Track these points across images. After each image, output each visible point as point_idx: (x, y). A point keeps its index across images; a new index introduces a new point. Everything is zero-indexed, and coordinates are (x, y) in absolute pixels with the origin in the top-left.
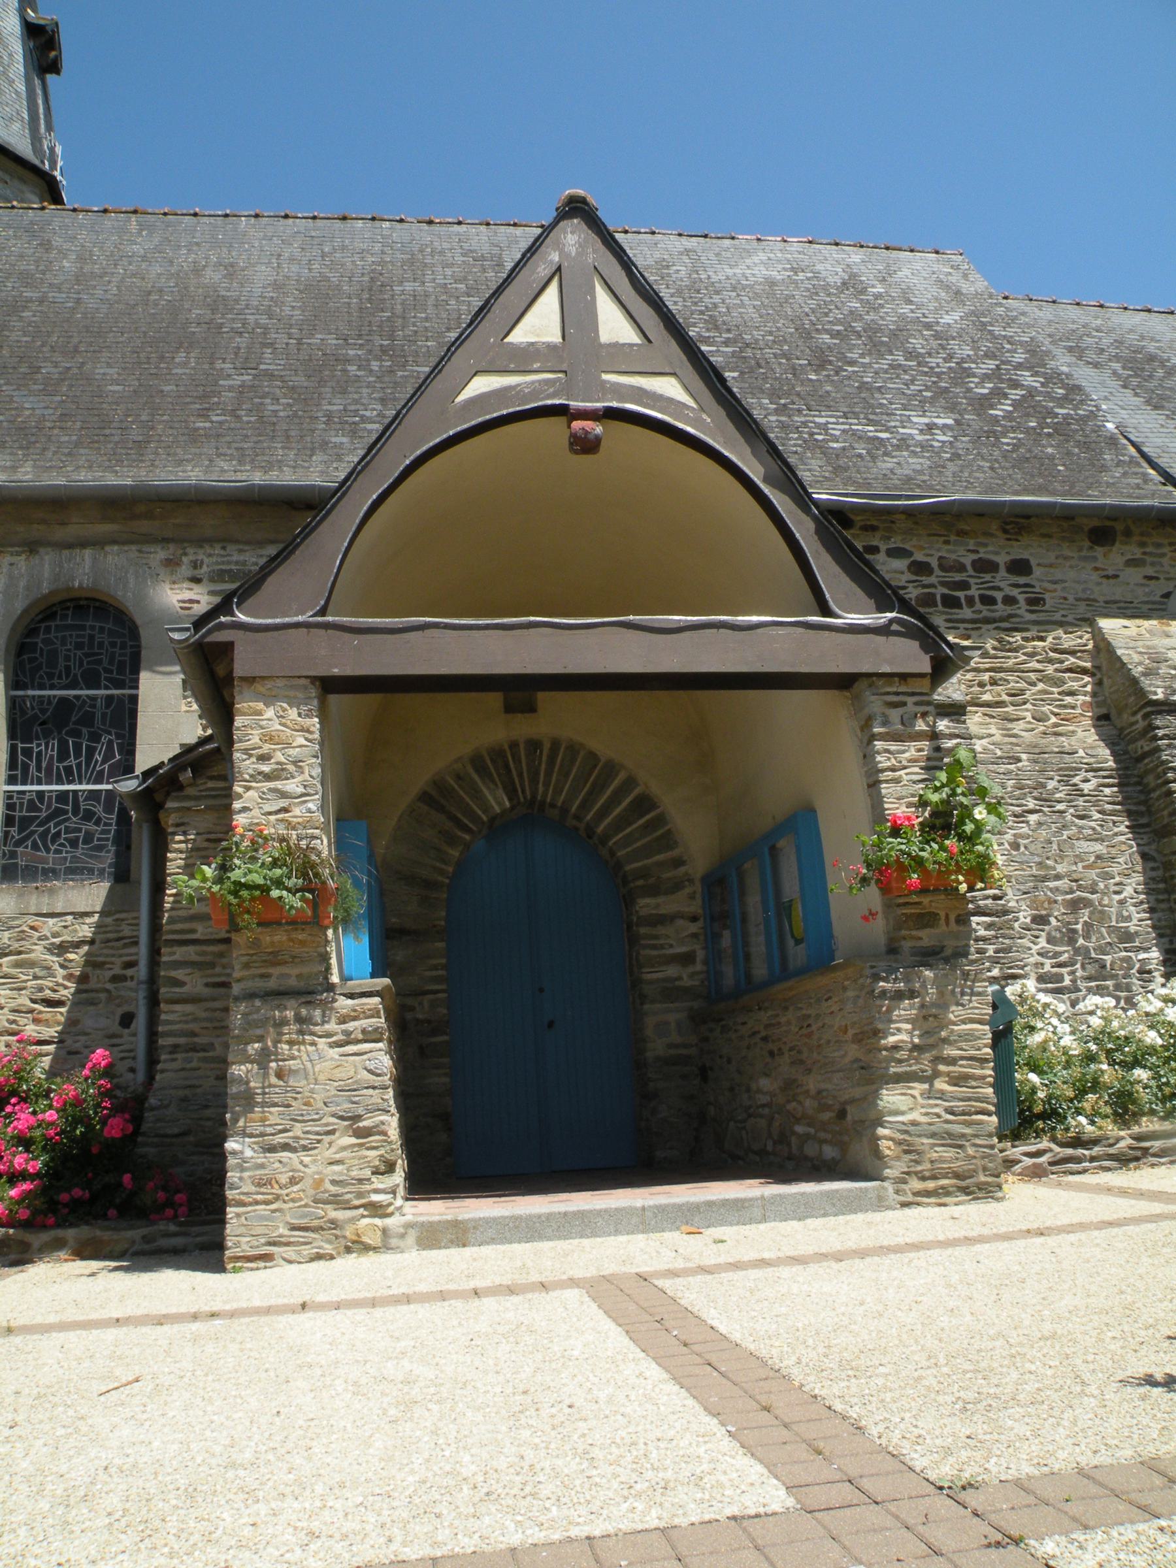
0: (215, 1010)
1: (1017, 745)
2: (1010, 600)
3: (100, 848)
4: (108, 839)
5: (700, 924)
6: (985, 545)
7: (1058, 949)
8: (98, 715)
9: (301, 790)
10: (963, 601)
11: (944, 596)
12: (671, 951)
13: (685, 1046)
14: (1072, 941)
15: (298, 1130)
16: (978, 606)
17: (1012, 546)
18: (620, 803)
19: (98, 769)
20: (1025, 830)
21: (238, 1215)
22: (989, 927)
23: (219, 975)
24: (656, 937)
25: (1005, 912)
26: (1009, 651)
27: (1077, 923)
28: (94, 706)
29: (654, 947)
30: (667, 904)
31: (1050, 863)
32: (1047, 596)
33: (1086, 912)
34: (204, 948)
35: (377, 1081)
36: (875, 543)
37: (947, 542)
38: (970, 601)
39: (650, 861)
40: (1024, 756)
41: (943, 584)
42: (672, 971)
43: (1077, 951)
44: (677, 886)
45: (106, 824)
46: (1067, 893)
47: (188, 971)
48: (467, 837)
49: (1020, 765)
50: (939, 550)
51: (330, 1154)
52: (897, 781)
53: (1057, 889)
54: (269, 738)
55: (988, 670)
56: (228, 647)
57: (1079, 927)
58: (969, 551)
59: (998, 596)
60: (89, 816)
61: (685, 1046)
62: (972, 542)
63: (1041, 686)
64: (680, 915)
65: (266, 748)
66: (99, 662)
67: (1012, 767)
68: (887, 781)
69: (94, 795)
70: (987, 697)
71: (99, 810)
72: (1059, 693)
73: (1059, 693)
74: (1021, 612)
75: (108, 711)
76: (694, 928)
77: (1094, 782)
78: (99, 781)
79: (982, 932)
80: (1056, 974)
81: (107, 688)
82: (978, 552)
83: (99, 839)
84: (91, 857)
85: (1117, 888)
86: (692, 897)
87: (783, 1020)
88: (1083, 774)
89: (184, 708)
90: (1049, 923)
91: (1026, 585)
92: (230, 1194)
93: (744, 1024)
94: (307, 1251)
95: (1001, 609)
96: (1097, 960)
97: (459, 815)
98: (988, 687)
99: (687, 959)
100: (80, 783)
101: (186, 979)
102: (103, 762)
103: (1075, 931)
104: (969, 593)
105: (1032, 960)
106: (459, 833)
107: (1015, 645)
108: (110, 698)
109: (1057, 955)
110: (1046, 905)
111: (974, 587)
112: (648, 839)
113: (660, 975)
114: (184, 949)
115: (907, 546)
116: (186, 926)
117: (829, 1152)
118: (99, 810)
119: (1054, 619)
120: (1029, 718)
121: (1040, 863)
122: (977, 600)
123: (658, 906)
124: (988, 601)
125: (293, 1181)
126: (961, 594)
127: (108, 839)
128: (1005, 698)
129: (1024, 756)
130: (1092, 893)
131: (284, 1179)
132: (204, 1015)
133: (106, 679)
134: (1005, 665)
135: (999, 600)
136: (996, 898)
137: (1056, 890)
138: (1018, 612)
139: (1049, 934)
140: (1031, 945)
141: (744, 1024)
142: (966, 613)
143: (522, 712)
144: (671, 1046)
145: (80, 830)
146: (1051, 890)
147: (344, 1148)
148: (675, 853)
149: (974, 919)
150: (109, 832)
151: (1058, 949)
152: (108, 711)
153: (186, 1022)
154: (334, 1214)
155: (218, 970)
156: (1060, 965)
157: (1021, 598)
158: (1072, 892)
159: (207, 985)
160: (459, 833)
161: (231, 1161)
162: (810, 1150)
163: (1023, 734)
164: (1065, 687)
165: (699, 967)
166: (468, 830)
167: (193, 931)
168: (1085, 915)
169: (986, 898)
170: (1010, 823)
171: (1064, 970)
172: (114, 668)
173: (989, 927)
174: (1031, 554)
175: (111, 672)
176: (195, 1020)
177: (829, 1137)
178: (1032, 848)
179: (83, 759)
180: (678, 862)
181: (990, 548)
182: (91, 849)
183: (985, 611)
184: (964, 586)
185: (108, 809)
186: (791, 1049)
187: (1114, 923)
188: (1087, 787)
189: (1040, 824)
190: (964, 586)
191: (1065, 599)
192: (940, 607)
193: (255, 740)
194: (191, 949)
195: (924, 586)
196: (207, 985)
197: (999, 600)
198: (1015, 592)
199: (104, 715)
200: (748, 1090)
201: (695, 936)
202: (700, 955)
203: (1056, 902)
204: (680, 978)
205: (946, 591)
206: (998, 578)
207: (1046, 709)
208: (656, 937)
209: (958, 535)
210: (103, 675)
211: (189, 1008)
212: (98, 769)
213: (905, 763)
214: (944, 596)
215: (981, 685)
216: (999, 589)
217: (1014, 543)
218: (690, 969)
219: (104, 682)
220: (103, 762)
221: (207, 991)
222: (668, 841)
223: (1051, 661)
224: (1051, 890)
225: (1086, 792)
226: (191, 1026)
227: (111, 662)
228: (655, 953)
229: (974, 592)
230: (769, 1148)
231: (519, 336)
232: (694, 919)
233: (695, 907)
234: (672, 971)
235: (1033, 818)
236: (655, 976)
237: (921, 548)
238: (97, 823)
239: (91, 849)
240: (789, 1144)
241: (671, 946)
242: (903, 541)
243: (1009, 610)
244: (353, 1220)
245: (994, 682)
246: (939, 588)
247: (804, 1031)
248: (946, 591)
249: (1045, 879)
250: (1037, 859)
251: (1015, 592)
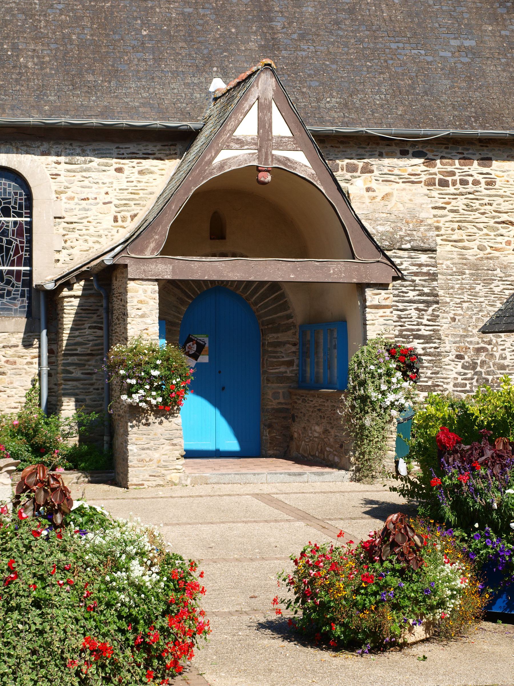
0: (86, 385)
1: (465, 265)
2: (476, 183)
3: (14, 299)
4: (18, 294)
5: (297, 347)
6: (468, 150)
7: (466, 371)
8: (10, 232)
9: (152, 322)
10: (450, 183)
11: (440, 180)
12: (283, 360)
13: (286, 404)
14: (474, 368)
15: (152, 443)
16: (458, 186)
17: (483, 150)
18: (263, 287)
19: (12, 259)
20: (460, 312)
21: (132, 471)
22: (429, 361)
23: (88, 370)
24: (276, 352)
25: (439, 354)
26: (471, 211)
27: (478, 359)
28: (7, 226)
29: (275, 357)
30: (282, 337)
31: (470, 329)
32: (498, 180)
33: (484, 354)
34: (81, 358)
35: (178, 428)
36: (407, 149)
37: (447, 148)
38: (454, 183)
39: (276, 316)
40: (467, 272)
41: (440, 172)
42: (282, 369)
43: (476, 373)
44: (288, 328)
45: (17, 287)
46: (476, 344)
47: (74, 367)
48: (190, 301)
49: (464, 276)
50: (441, 152)
51: (163, 452)
52: (373, 324)
53: (471, 342)
54: (141, 302)
55: (457, 222)
56: (126, 266)
57: (479, 362)
58: (458, 153)
59: (470, 179)
60: (8, 282)
61: (286, 404)
62: (460, 148)
63: (485, 231)
64: (288, 342)
65: (140, 306)
66: (10, 203)
67: (459, 277)
68: (370, 325)
69: (10, 272)
70: (454, 237)
71: (13, 280)
72: (495, 236)
73: (495, 236)
74: (482, 189)
75: (15, 229)
76: (294, 349)
77: (502, 287)
78: (12, 265)
79: (426, 364)
80: (463, 383)
81: (14, 217)
82: (463, 154)
83: (14, 294)
84: (10, 303)
85: (502, 343)
86: (295, 334)
87: (326, 404)
88: (496, 283)
89: (55, 232)
90: (464, 359)
91: (487, 174)
92: (130, 464)
93: (312, 401)
94: (155, 483)
95: (470, 187)
96: (485, 378)
97: (187, 291)
98: (457, 231)
99: (290, 363)
100: (4, 266)
101: (73, 371)
102: (14, 256)
103: (477, 363)
104: (454, 178)
105: (452, 376)
106: (187, 300)
107: (474, 208)
108: (15, 223)
109: (465, 374)
110: (464, 350)
111: (458, 174)
112: (274, 306)
113: (277, 371)
114: (72, 357)
115: (424, 150)
116: (73, 347)
117: (337, 459)
118: (13, 280)
119: (498, 193)
120: (476, 249)
121: (465, 329)
122: (458, 182)
123: (278, 338)
124: (464, 182)
125: (151, 460)
126: (449, 179)
127: (18, 294)
128: (465, 237)
129: (467, 272)
130: (489, 345)
131: (148, 460)
132: (82, 386)
133: (13, 212)
134: (467, 219)
135: (470, 182)
136: (435, 348)
137: (471, 343)
138: (479, 189)
139: (463, 364)
140: (453, 369)
141: (312, 401)
142: (451, 189)
143: (219, 239)
144: (279, 403)
145: (5, 290)
146: (468, 342)
147: (167, 450)
148: (288, 312)
149: (423, 358)
150: (18, 291)
151: (466, 371)
152: (15, 229)
153: (74, 389)
154: (163, 472)
155: (87, 367)
156: (465, 379)
157: (483, 181)
158: (478, 343)
159: (82, 373)
160: (187, 300)
161: (130, 453)
162: (331, 458)
163: (470, 258)
164: (498, 232)
165: (295, 368)
166: (189, 297)
167: (76, 350)
168: (483, 356)
169: (431, 348)
170: (453, 308)
171: (467, 382)
172: (17, 206)
173: (429, 361)
174: (493, 155)
175: (15, 208)
176: (78, 388)
177: (337, 453)
178: (462, 320)
179: (4, 253)
180: (289, 317)
181: (470, 151)
182: (10, 299)
183: (461, 189)
184: (453, 174)
185: (18, 279)
186: (328, 417)
187: (497, 360)
188: (497, 290)
189: (468, 308)
190: (453, 174)
191: (508, 181)
192: (437, 186)
193: (135, 303)
194: (75, 357)
195: (431, 174)
196: (82, 373)
197: (470, 182)
198: (480, 178)
199: (13, 231)
200: (311, 429)
201: (294, 352)
202: (296, 362)
203: (469, 348)
204: (286, 372)
205: (442, 177)
206: (472, 169)
207: (486, 244)
208: (276, 352)
209: (454, 144)
210: (12, 210)
211: (75, 383)
212: (12, 259)
213: (378, 318)
214: (440, 180)
215: (453, 230)
216: (472, 176)
217: (485, 148)
218: (291, 369)
219: (12, 214)
220: (14, 256)
221: (82, 376)
222: (285, 306)
223: (493, 217)
224: (468, 342)
225: (496, 292)
226: (76, 391)
227: (15, 203)
228: (275, 360)
229: (457, 178)
230: (317, 455)
231: (239, 133)
232: (295, 345)
233: (295, 339)
234: (282, 369)
235: (465, 305)
236: (272, 371)
237: (432, 151)
238: (13, 286)
239: (10, 299)
240: (324, 454)
241: (283, 357)
242: (422, 147)
243: (475, 188)
244: (169, 474)
245: (460, 228)
246: (438, 175)
247: (332, 412)
248: (442, 177)
249: (466, 336)
250: (463, 326)
251: (480, 178)
